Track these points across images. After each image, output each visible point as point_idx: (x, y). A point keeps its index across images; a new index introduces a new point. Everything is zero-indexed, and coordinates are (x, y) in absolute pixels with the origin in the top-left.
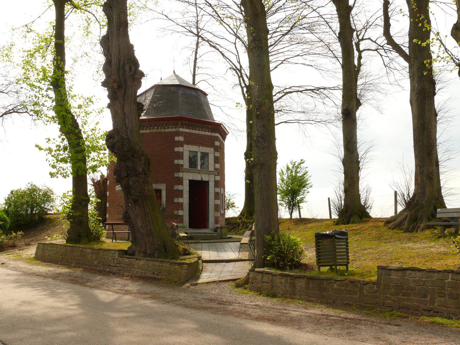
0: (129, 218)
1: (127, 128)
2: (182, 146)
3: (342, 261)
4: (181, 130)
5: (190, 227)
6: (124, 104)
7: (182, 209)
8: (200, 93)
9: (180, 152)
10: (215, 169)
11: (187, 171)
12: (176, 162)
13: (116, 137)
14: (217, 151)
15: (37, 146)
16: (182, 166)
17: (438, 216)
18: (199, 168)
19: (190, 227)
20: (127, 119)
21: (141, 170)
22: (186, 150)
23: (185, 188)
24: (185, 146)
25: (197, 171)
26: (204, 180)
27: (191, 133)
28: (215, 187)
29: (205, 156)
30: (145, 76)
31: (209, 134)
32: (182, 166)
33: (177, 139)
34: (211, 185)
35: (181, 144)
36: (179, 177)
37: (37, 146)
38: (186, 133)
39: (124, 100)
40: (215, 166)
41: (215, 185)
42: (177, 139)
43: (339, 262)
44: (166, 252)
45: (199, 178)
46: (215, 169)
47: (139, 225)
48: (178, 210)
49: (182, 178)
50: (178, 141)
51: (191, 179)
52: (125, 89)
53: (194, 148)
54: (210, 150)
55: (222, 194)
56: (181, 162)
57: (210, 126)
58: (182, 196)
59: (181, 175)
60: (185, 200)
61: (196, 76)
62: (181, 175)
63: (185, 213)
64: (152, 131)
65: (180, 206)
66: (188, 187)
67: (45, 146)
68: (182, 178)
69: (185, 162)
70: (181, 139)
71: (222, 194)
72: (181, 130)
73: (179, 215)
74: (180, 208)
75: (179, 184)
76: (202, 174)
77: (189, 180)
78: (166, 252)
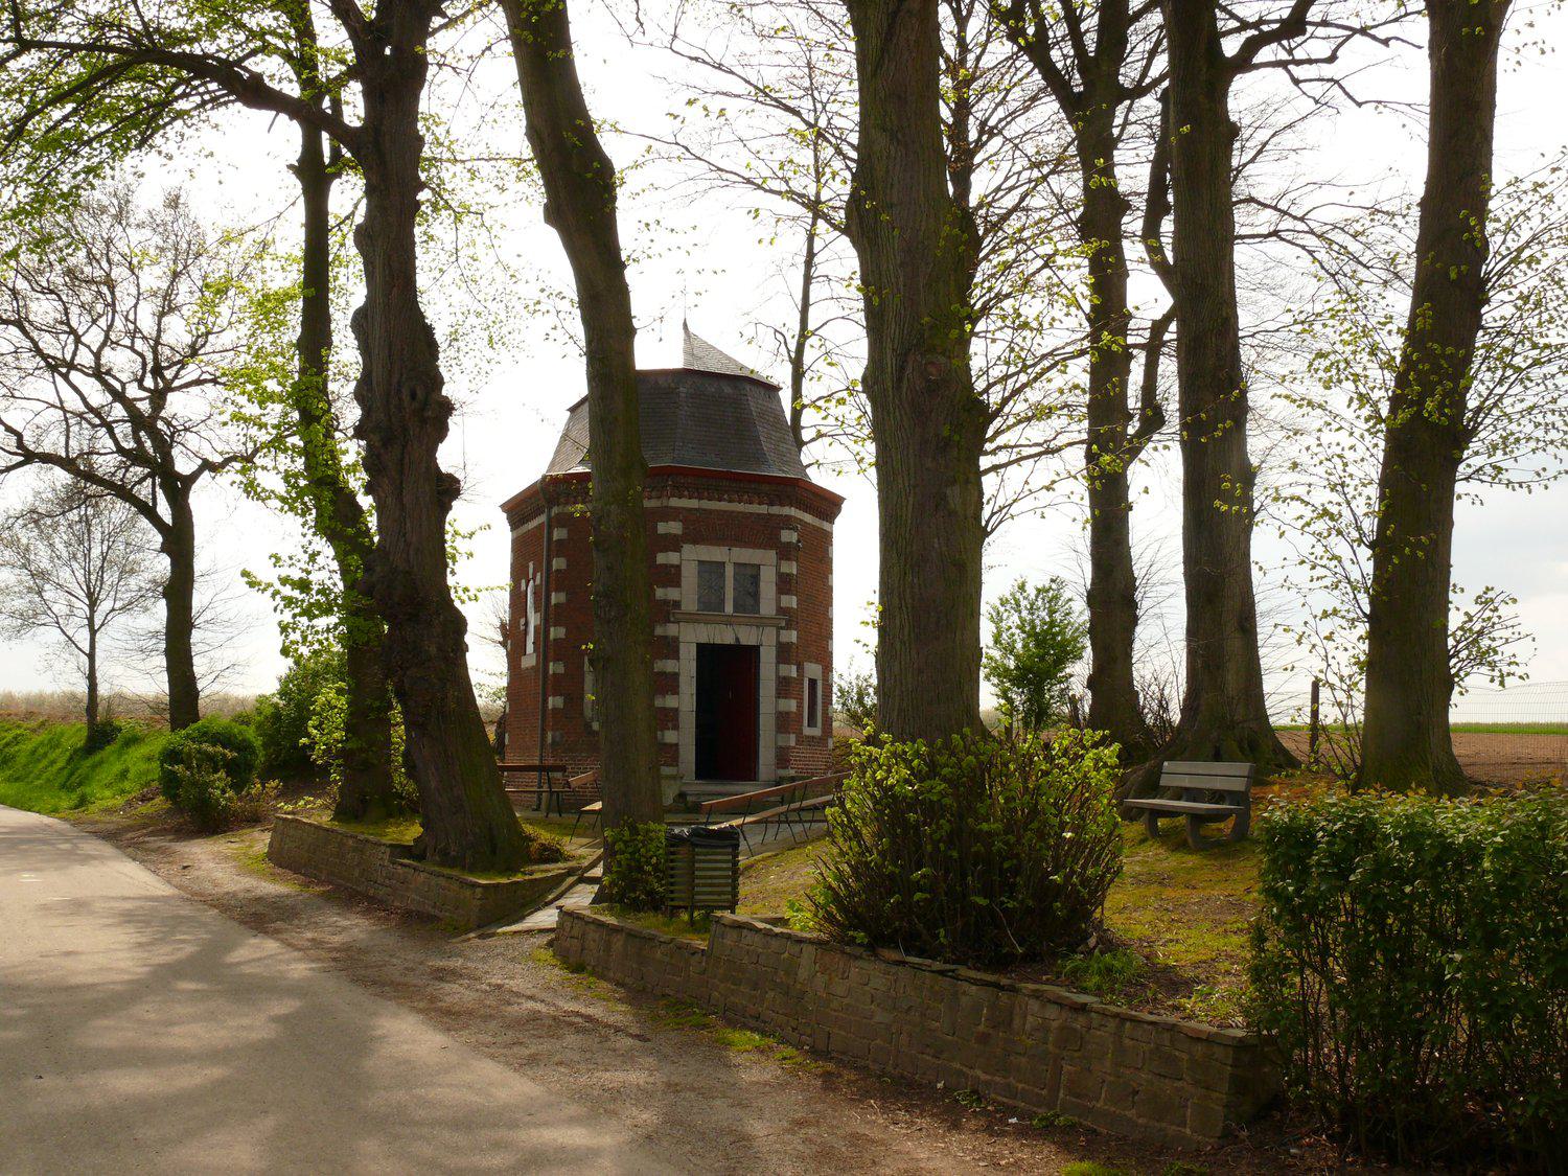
0: (414, 767)
1: (408, 544)
2: (678, 549)
3: (716, 897)
4: (675, 502)
5: (698, 777)
6: (401, 483)
7: (676, 727)
8: (748, 387)
9: (672, 566)
10: (781, 610)
11: (692, 619)
12: (660, 593)
13: (378, 569)
14: (789, 559)
15: (245, 574)
16: (677, 604)
17: (1164, 781)
18: (729, 608)
19: (698, 777)
20: (408, 521)
21: (433, 650)
22: (690, 558)
23: (686, 666)
24: (687, 548)
25: (725, 619)
26: (744, 641)
27: (705, 510)
28: (778, 663)
29: (749, 578)
30: (456, 406)
31: (763, 509)
32: (677, 604)
33: (663, 528)
34: (768, 657)
35: (673, 543)
36: (666, 637)
37: (245, 574)
39: (402, 473)
40: (778, 601)
41: (778, 657)
42: (663, 528)
43: (700, 901)
44: (494, 852)
45: (729, 640)
46: (781, 610)
47: (433, 785)
48: (664, 728)
49: (676, 640)
50: (666, 536)
51: (704, 640)
52: (404, 447)
53: (716, 553)
54: (767, 563)
55: (813, 683)
56: (672, 594)
57: (766, 488)
58: (675, 690)
59: (672, 630)
60: (685, 701)
61: (811, 309)
62: (672, 630)
63: (684, 738)
65: (670, 718)
66: (694, 664)
67: (268, 574)
68: (678, 638)
69: (687, 594)
70: (674, 528)
71: (813, 683)
72: (675, 502)
73: (665, 744)
74: (670, 725)
75: (667, 657)
76: (736, 628)
77: (699, 646)
78: (494, 852)
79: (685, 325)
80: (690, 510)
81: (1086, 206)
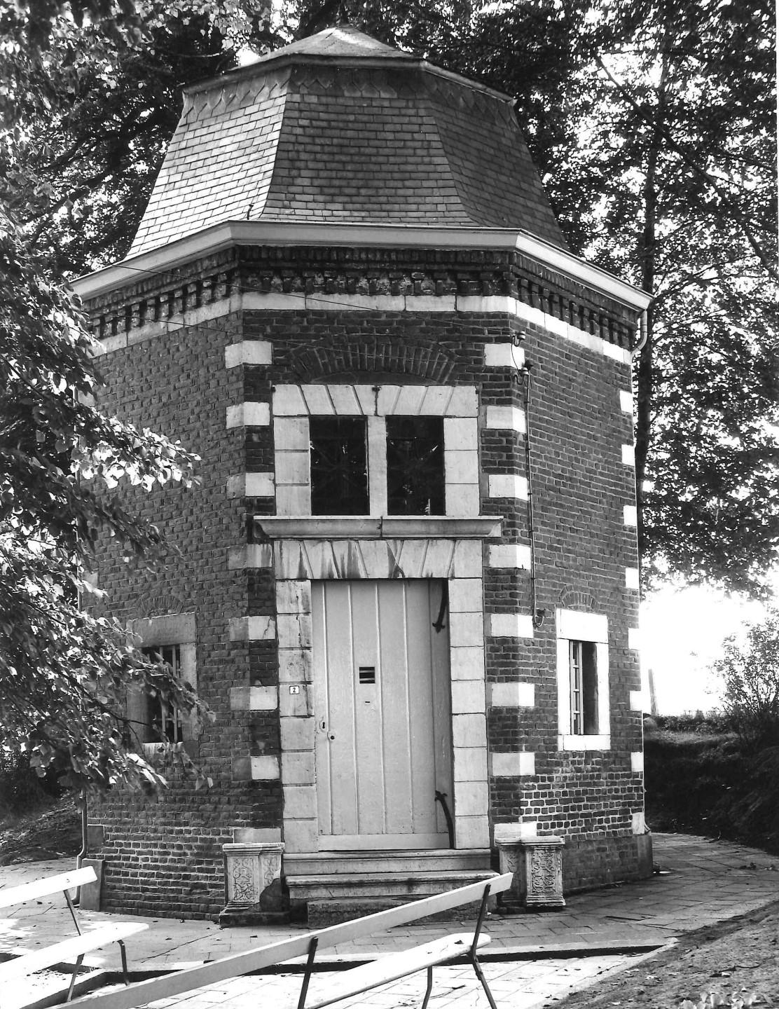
10: (490, 505)
31: (445, 304)
38: (286, 316)
46: (490, 505)
57: (251, 73)
64: (135, 334)
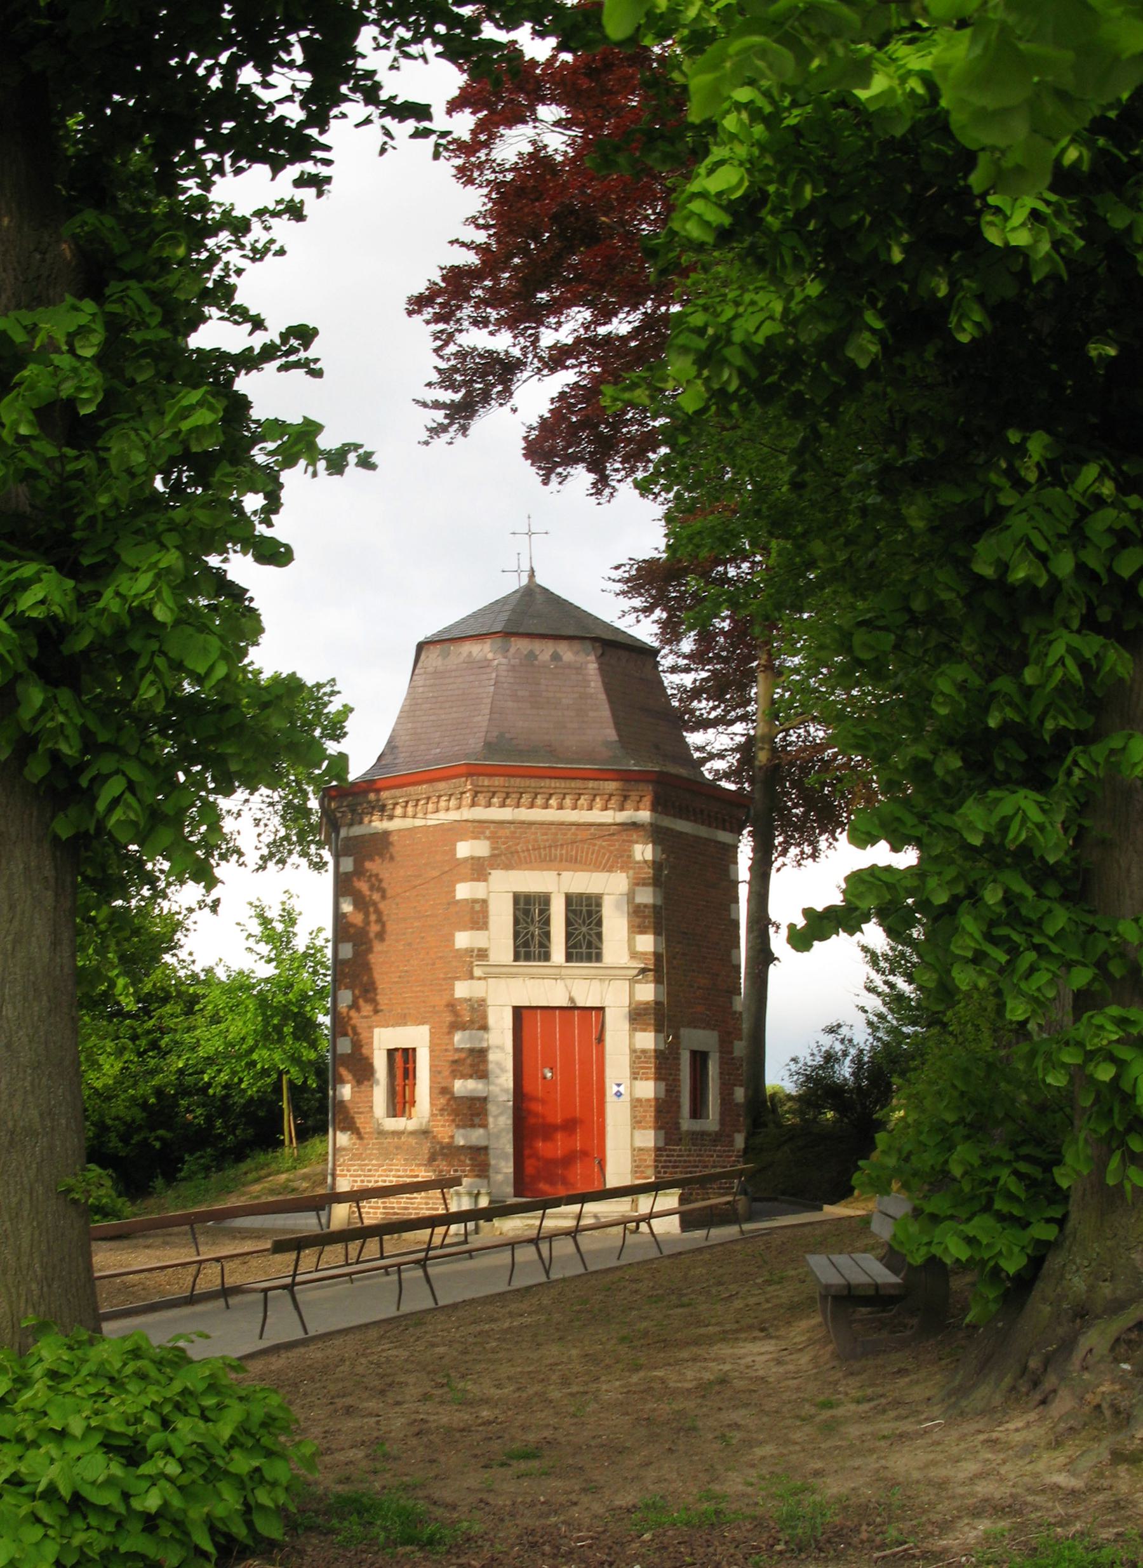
11: (498, 973)
16: (483, 954)
35: (479, 869)
53: (532, 881)
79: (418, 402)
80: (501, 823)
81: (950, 331)
